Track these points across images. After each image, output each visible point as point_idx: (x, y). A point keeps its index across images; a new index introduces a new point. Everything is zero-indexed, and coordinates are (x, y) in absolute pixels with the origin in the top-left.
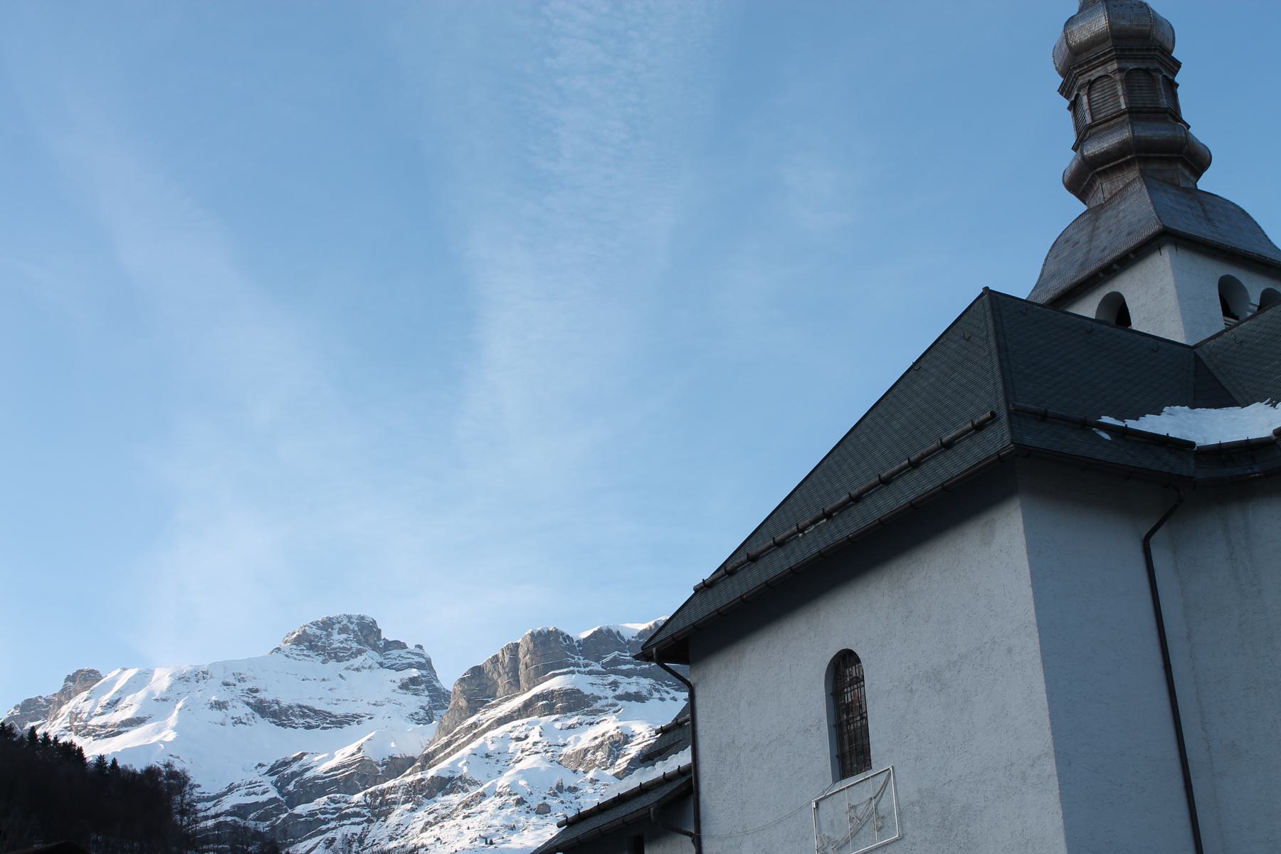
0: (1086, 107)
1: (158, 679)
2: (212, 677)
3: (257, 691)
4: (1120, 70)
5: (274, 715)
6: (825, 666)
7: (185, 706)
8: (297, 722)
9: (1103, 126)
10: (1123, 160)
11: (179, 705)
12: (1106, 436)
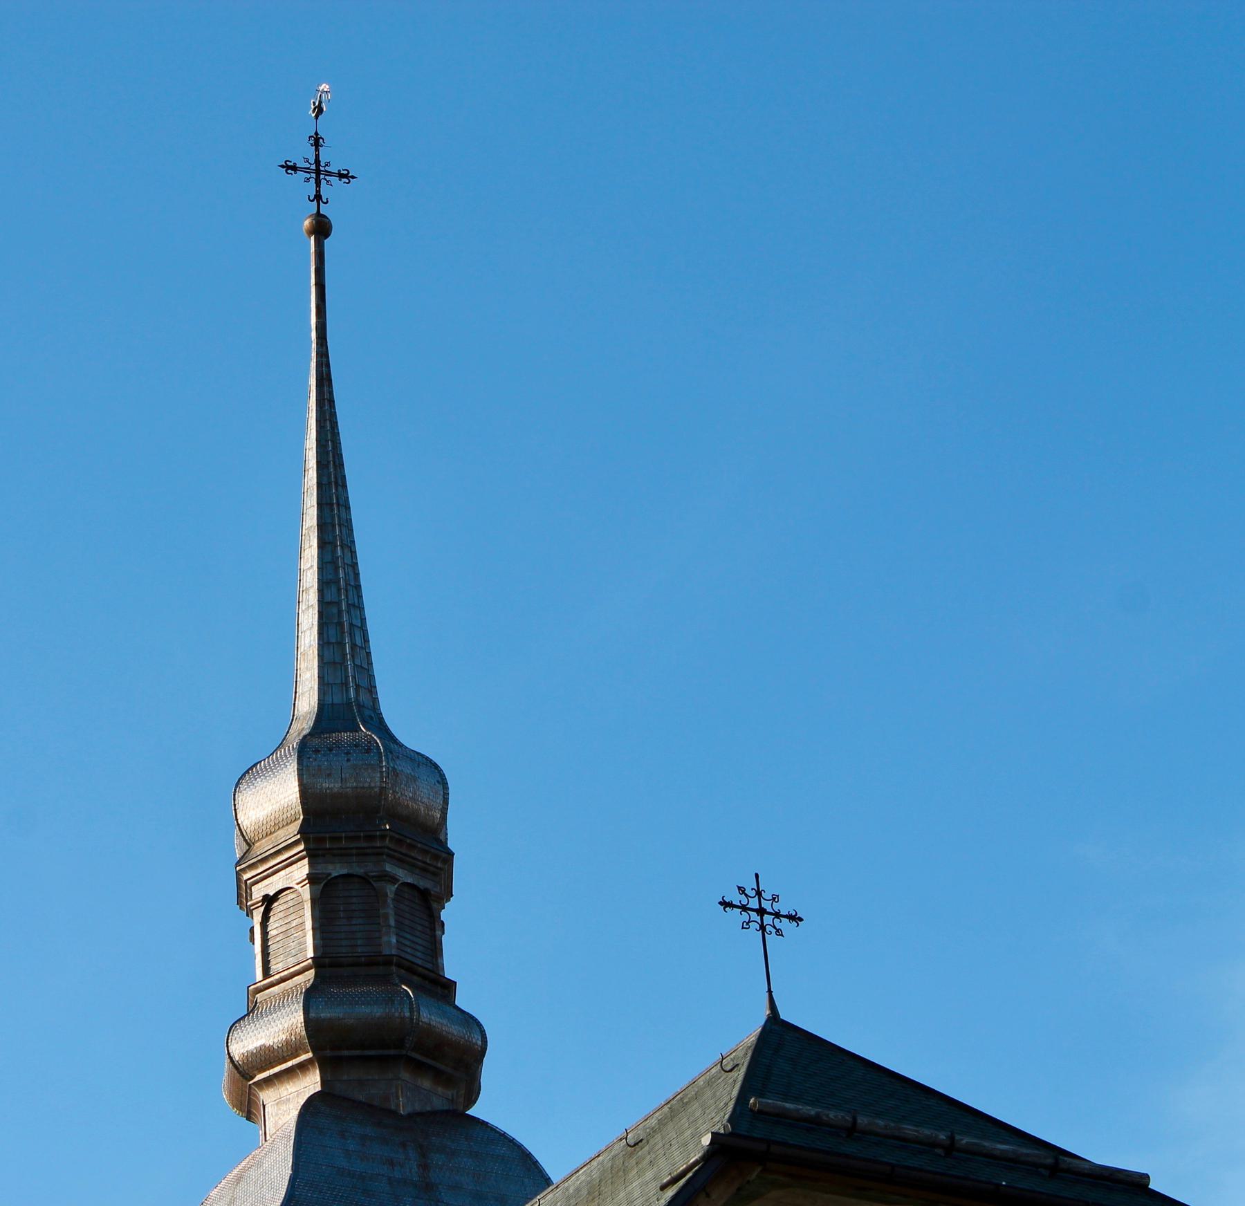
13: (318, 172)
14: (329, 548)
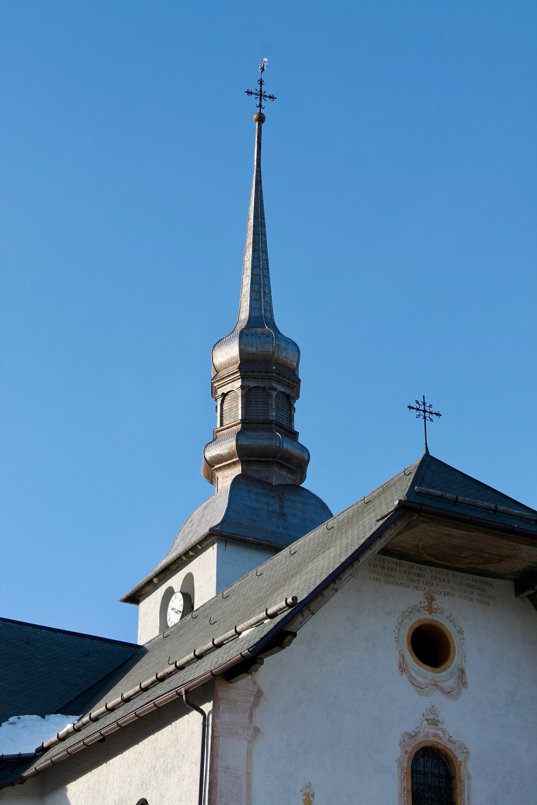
13: (261, 95)
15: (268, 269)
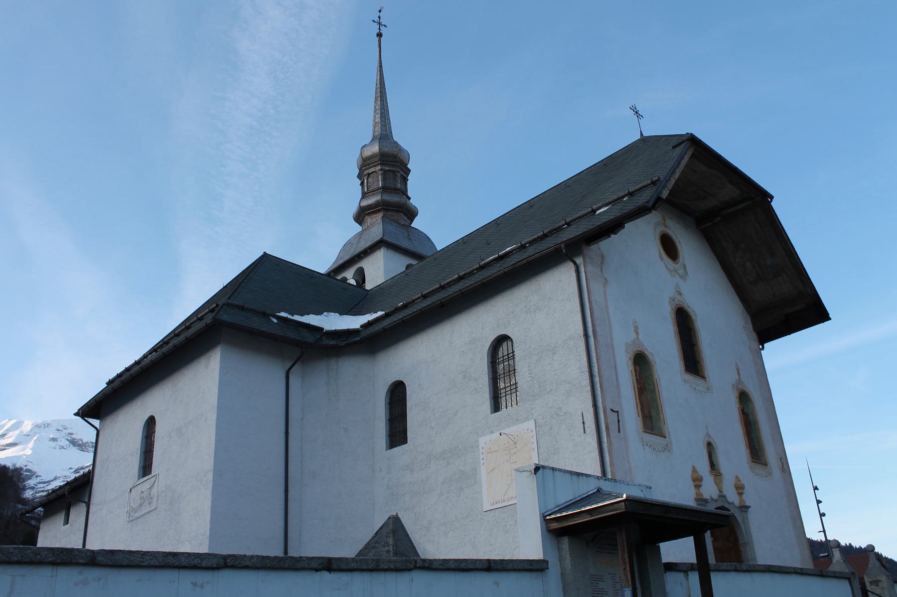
0: (365, 184)
1: (26, 425)
2: (51, 426)
3: (72, 434)
4: (381, 170)
5: (79, 445)
6: (144, 423)
7: (37, 439)
8: (90, 449)
9: (371, 193)
10: (377, 209)
11: (35, 438)
12: (275, 321)
13: (380, 24)
14: (382, 102)
15: (388, 111)
